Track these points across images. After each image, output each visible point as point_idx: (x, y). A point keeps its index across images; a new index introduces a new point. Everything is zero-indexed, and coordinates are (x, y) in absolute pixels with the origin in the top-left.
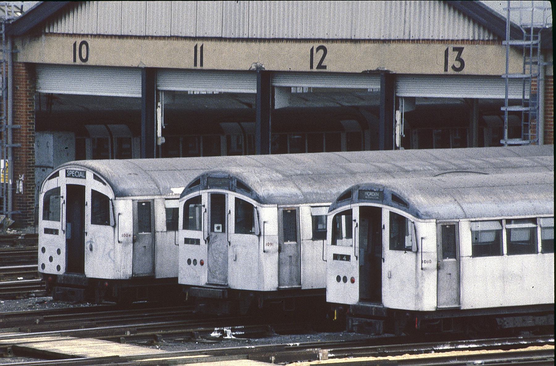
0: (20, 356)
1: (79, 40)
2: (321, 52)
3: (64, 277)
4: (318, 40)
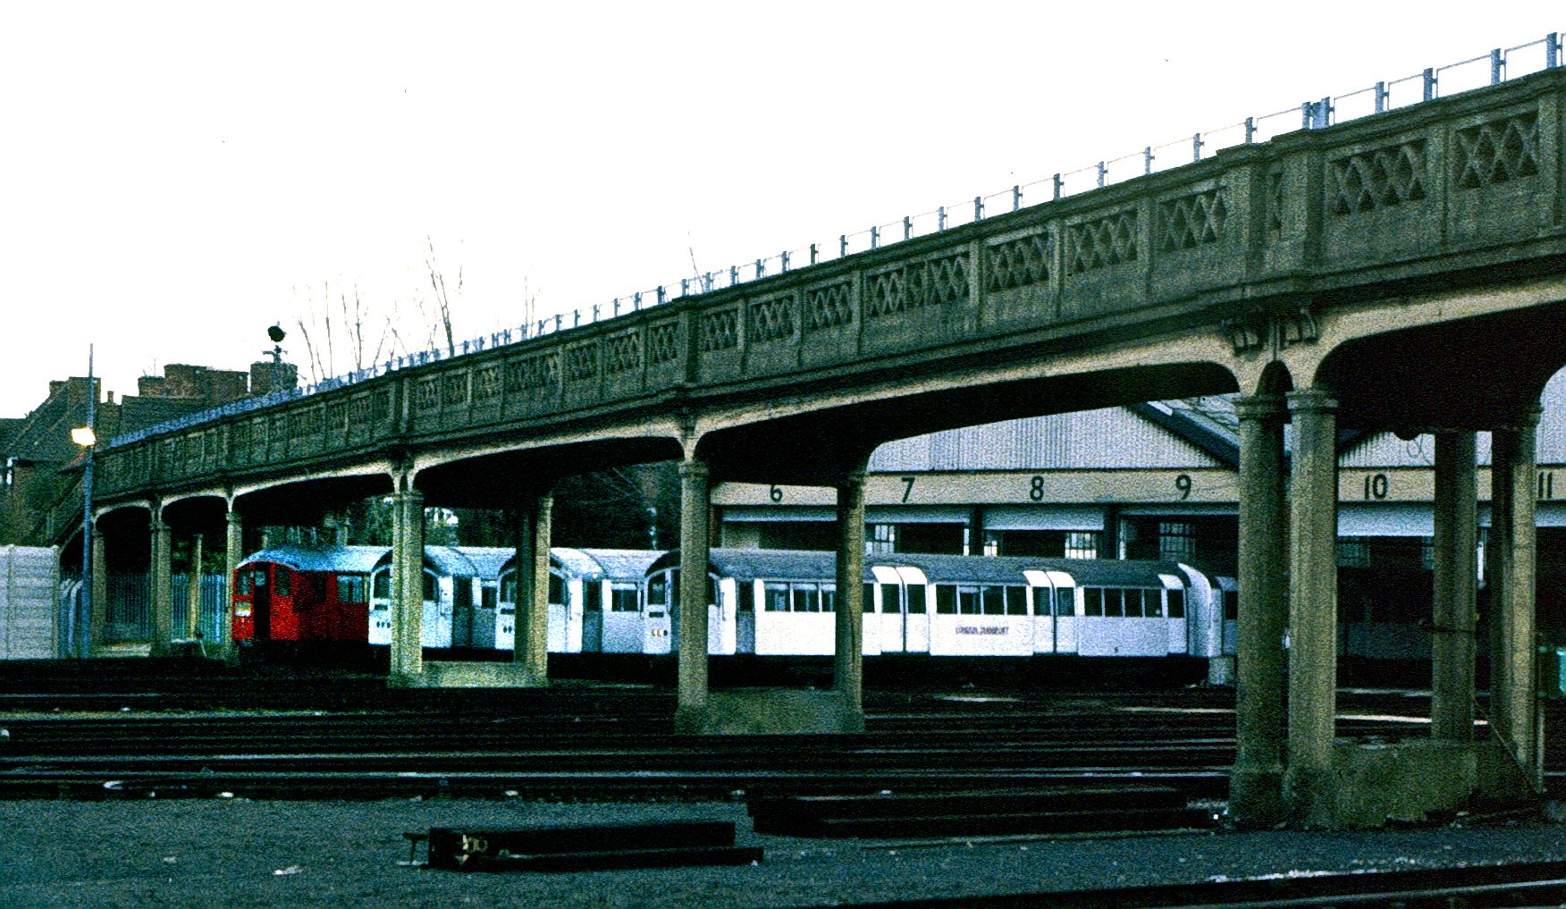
0: (775, 684)
1: (1374, 474)
4: (1374, 469)
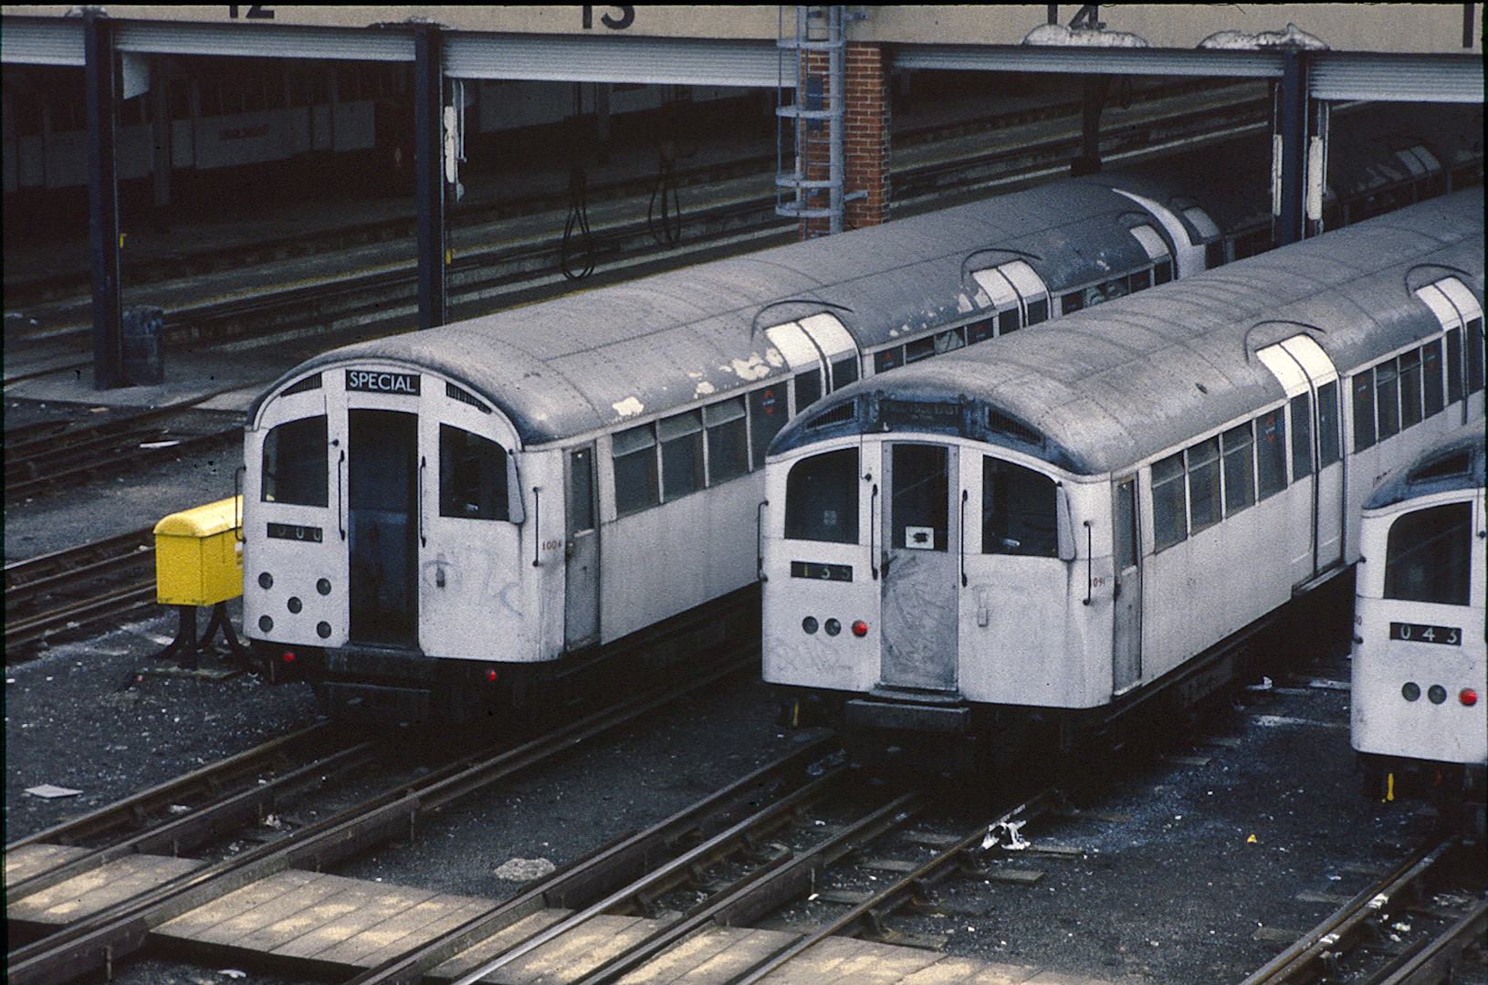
3: (350, 656)
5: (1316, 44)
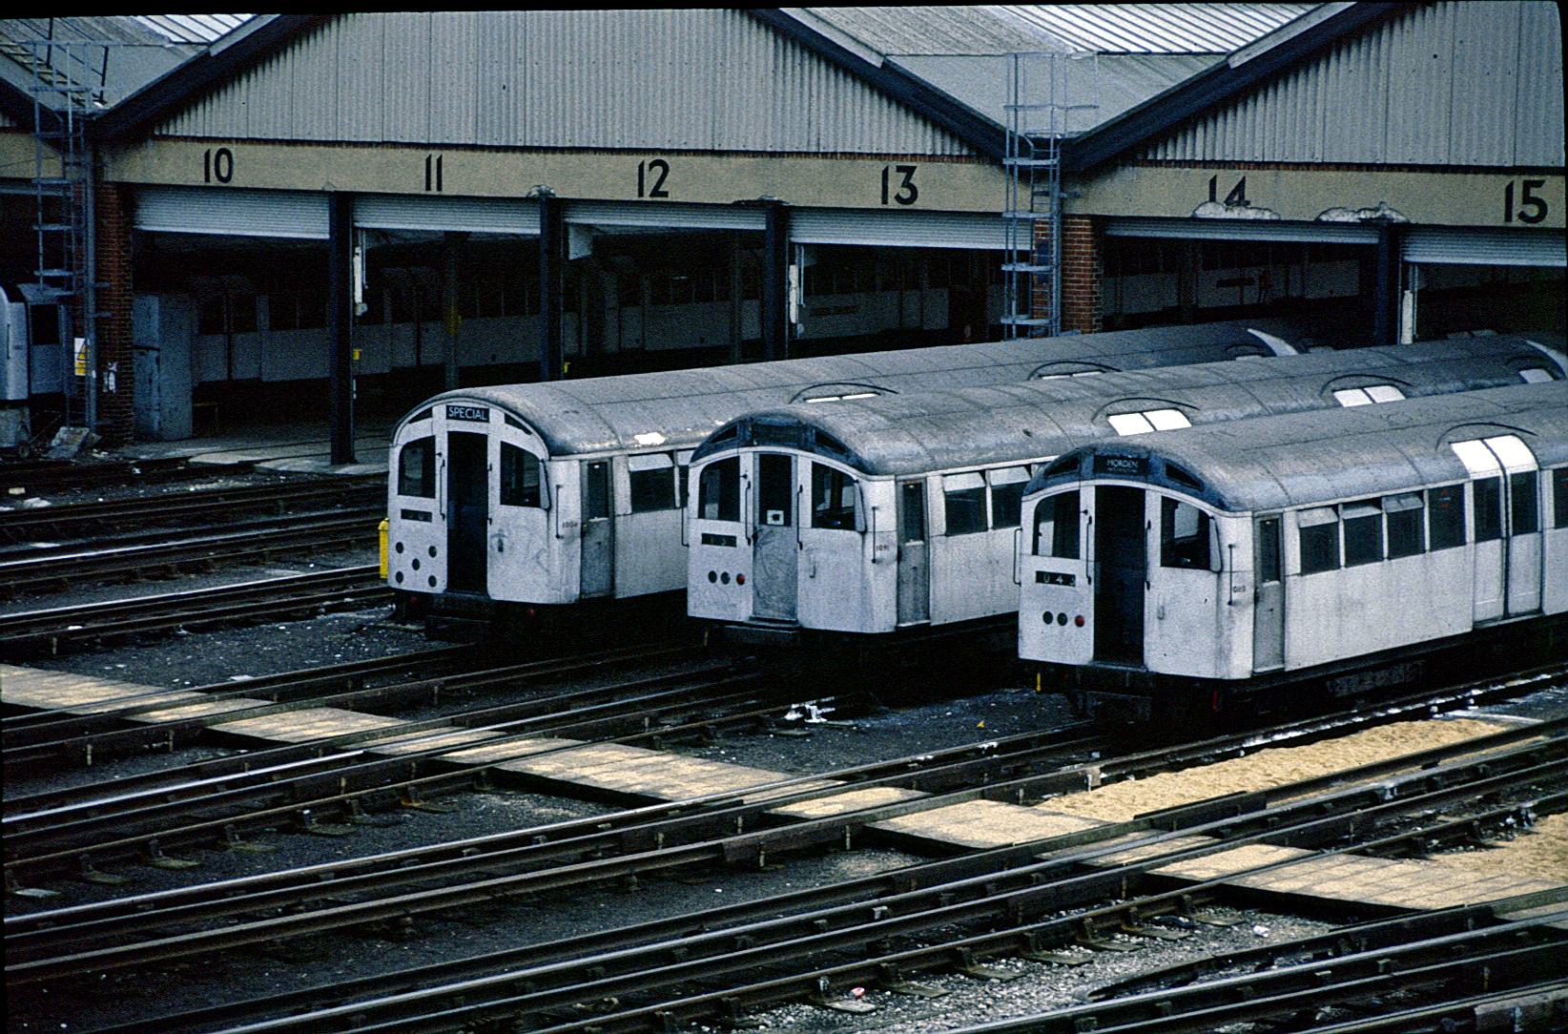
1: (215, 148)
2: (659, 169)
4: (653, 151)
5: (1401, 219)
